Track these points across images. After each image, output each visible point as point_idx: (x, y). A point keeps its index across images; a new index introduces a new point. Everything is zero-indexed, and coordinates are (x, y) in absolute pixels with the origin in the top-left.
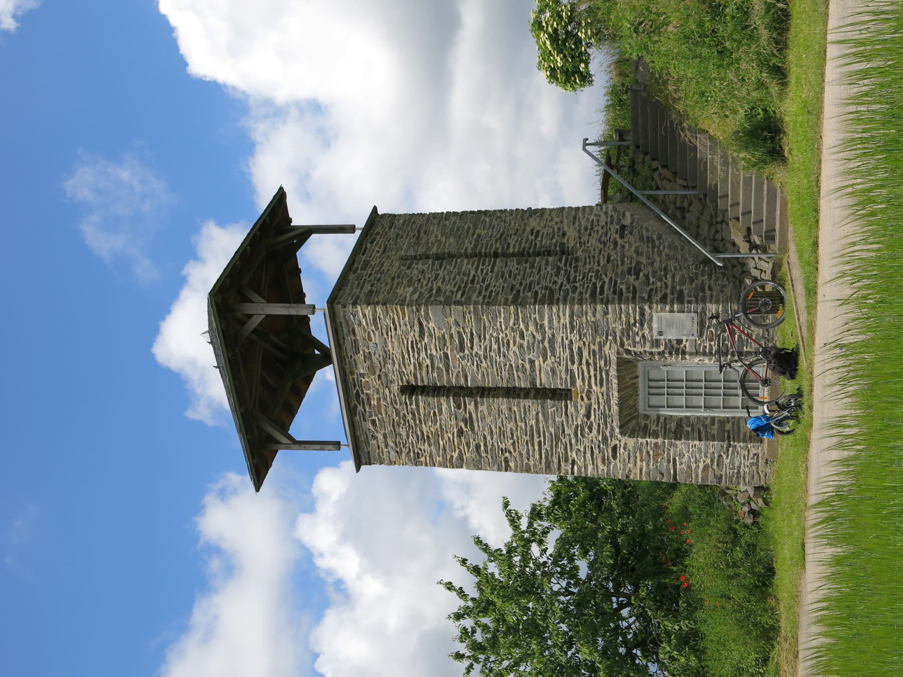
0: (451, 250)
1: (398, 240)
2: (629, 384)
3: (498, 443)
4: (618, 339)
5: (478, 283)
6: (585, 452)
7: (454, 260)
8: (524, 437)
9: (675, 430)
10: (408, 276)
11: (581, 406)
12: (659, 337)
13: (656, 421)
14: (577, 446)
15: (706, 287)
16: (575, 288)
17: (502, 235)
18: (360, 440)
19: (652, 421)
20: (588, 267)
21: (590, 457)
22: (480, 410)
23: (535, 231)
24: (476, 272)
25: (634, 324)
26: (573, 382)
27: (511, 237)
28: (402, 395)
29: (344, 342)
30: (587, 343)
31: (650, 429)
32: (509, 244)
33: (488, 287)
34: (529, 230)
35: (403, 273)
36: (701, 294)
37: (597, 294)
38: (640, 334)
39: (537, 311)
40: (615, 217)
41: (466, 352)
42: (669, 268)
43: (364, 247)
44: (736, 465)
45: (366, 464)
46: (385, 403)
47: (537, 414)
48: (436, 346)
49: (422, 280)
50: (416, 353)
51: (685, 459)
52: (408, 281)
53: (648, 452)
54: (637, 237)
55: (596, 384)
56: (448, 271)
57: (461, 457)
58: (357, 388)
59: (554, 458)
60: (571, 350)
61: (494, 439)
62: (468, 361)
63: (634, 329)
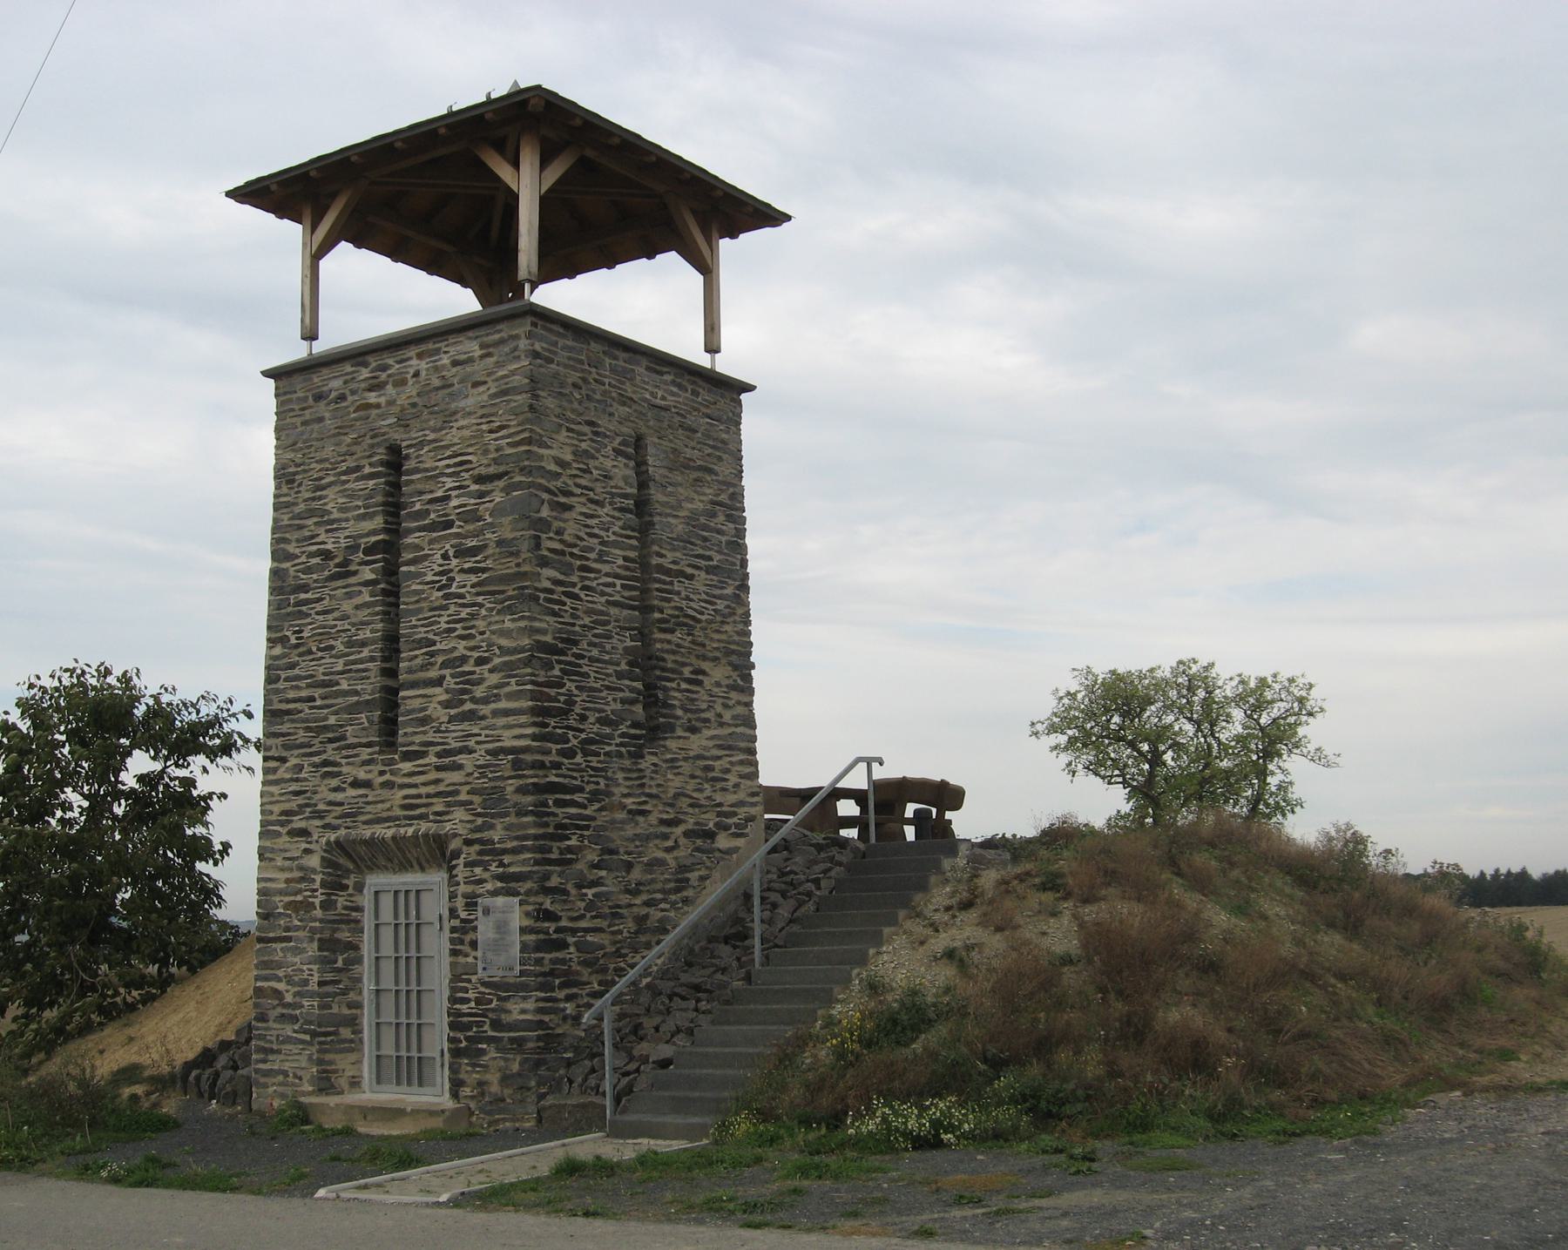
0: (657, 527)
1: (680, 431)
2: (409, 855)
3: (310, 624)
6: (297, 780)
7: (636, 534)
8: (321, 670)
9: (339, 941)
10: (598, 451)
12: (480, 909)
14: (309, 765)
15: (575, 990)
17: (693, 618)
18: (314, 376)
19: (352, 899)
20: (620, 776)
21: (290, 789)
22: (363, 589)
23: (700, 677)
24: (607, 575)
25: (501, 864)
26: (407, 756)
27: (689, 635)
28: (387, 448)
29: (470, 338)
30: (470, 779)
31: (337, 895)
32: (672, 631)
33: (576, 597)
35: (606, 441)
36: (557, 981)
37: (557, 796)
38: (486, 875)
39: (521, 688)
40: (735, 820)
41: (455, 562)
42: (617, 922)
43: (665, 369)
44: (283, 1047)
46: (372, 416)
47: (356, 693)
48: (465, 505)
50: (452, 470)
51: (290, 959)
53: (299, 892)
54: (688, 862)
55: (406, 797)
56: (609, 522)
57: (290, 557)
58: (397, 366)
59: (288, 725)
60: (461, 751)
61: (317, 617)
63: (494, 864)
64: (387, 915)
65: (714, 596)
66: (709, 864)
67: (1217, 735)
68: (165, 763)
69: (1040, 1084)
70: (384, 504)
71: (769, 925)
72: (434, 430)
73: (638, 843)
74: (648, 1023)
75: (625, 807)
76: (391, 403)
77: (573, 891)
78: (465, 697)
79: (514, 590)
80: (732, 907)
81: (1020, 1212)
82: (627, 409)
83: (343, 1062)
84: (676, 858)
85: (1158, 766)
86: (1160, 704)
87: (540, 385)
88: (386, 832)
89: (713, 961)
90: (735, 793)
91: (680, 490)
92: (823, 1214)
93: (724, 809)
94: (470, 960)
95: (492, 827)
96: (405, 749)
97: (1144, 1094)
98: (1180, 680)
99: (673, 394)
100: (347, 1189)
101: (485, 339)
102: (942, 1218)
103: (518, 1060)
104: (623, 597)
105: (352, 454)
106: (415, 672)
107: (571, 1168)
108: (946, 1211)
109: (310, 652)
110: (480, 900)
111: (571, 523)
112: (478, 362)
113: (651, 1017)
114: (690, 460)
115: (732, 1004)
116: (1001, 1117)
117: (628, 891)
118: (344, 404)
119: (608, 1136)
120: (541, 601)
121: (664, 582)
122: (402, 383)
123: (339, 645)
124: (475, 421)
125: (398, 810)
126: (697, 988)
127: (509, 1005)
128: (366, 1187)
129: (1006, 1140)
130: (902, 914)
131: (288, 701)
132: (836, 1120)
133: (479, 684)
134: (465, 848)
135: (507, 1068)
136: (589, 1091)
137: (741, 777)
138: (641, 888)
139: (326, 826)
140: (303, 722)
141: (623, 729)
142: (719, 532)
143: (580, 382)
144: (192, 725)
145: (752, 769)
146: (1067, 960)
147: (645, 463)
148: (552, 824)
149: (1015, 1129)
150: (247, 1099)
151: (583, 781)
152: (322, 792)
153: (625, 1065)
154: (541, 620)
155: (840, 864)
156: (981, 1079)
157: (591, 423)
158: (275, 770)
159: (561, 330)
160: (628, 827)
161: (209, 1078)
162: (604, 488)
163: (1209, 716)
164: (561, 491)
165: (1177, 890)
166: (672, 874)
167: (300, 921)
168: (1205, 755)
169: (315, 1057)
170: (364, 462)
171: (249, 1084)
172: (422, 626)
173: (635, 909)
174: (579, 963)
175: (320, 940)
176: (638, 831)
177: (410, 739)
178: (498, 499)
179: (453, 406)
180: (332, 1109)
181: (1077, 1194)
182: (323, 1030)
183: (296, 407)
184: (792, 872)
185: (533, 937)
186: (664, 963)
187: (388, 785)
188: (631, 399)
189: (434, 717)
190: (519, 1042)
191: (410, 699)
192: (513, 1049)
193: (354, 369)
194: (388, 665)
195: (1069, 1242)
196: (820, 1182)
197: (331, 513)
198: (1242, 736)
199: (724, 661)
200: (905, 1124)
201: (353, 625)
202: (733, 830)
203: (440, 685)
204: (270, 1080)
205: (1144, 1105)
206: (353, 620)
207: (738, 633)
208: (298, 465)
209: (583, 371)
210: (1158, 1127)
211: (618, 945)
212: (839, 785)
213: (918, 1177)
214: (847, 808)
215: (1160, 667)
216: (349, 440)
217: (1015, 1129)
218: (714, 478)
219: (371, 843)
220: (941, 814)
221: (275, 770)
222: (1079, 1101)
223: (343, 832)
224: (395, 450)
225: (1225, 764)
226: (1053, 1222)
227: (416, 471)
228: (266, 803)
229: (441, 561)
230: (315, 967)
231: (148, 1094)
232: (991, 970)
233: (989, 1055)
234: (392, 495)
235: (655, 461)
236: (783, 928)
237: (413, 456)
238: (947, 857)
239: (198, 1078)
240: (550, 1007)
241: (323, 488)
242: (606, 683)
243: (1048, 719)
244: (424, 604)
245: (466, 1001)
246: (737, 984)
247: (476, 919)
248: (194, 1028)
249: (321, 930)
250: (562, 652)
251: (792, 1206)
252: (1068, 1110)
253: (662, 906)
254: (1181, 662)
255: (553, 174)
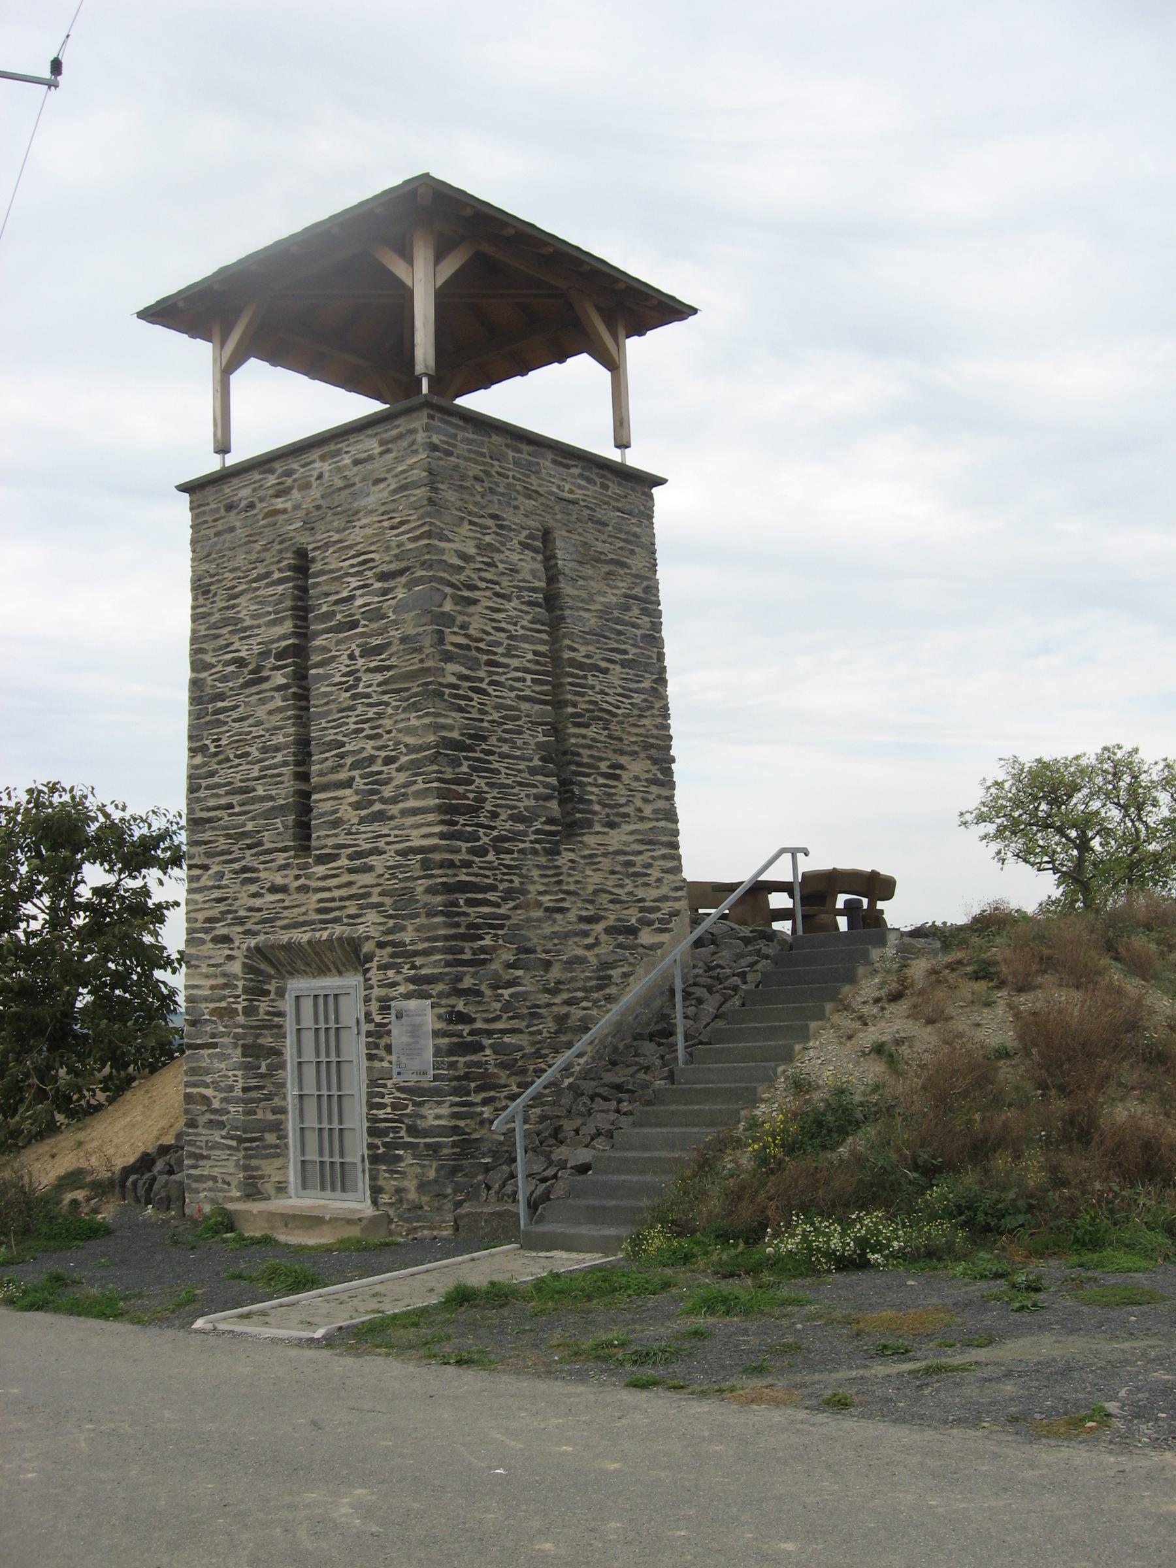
2: (326, 960)
3: (228, 731)
4: (390, 938)
5: (491, 673)
6: (219, 887)
7: (546, 628)
8: (239, 776)
9: (261, 1046)
10: (503, 544)
11: (286, 876)
12: (393, 1012)
13: (275, 1010)
15: (492, 1093)
16: (481, 852)
17: (609, 712)
18: (224, 487)
19: (274, 1004)
20: (535, 873)
21: (213, 896)
22: (276, 694)
23: (618, 772)
24: (516, 669)
25: (413, 967)
26: (322, 860)
27: (605, 729)
29: (369, 436)
31: (259, 1001)
32: (587, 726)
34: (621, 762)
35: (512, 534)
36: (473, 1085)
37: (469, 895)
38: (399, 978)
40: (659, 915)
41: (361, 661)
42: (536, 1022)
45: (191, 502)
47: (272, 798)
48: (368, 604)
49: (492, 569)
52: (490, 545)
53: (223, 998)
54: (610, 959)
55: (321, 901)
56: (517, 617)
57: (207, 667)
58: (302, 470)
61: (233, 724)
62: (348, 666)
63: (407, 966)
64: (308, 1021)
65: (631, 690)
66: (632, 961)
67: (1144, 819)
68: (120, 875)
69: (976, 1196)
70: (293, 608)
71: (694, 1020)
72: (338, 532)
73: (556, 941)
74: (568, 1126)
75: (542, 904)
76: (296, 507)
77: (489, 993)
78: (375, 797)
79: (418, 686)
80: (657, 1004)
81: (955, 1369)
82: (534, 503)
83: (268, 1168)
84: (597, 955)
85: (1087, 851)
86: (1085, 791)
87: (438, 478)
88: (302, 936)
89: (637, 1059)
90: (658, 887)
91: (592, 583)
92: (723, 1367)
93: (646, 904)
94: (385, 1064)
95: (403, 929)
96: (318, 852)
97: (1093, 1206)
98: (1106, 766)
99: (581, 487)
100: (225, 1320)
101: (384, 436)
102: (862, 1378)
103: (434, 1167)
104: (533, 691)
105: (262, 561)
106: (326, 774)
107: (462, 1297)
108: (866, 1367)
109: (228, 760)
110: (393, 1003)
111: (476, 617)
112: (377, 459)
113: (572, 1119)
114: (601, 553)
115: (654, 1105)
116: (934, 1233)
117: (547, 991)
118: (252, 513)
119: (521, 1248)
120: (446, 697)
121: (578, 677)
122: (307, 486)
123: (255, 753)
124: (376, 519)
125: (313, 913)
126: (619, 1088)
127: (424, 1111)
128: (247, 1316)
129: (940, 1259)
130: (829, 1006)
131: (209, 809)
132: (754, 1235)
133: (387, 784)
134: (378, 951)
135: (423, 1175)
136: (506, 1198)
137: (664, 871)
138: (561, 987)
139: (247, 932)
140: (223, 829)
141: (537, 825)
142: (634, 625)
143: (482, 474)
144: (143, 837)
145: (675, 863)
146: (1003, 1053)
147: (554, 557)
148: (464, 924)
149: (950, 1247)
150: (180, 1203)
151: (495, 880)
152: (242, 898)
153: (544, 1171)
154: (446, 716)
155: (767, 957)
156: (911, 1188)
157: (494, 517)
158: (197, 878)
159: (461, 423)
160: (545, 925)
161: (145, 1183)
162: (511, 581)
163: (1136, 802)
164: (464, 585)
165: (1116, 975)
166: (593, 971)
167: (225, 1027)
168: (1134, 841)
169: (241, 1163)
170: (273, 568)
171: (182, 1187)
172: (332, 728)
173: (555, 1009)
174: (496, 1065)
175: (243, 1046)
176: (556, 929)
177: (323, 842)
178: (401, 596)
179: (355, 505)
180: (255, 1215)
181: (1021, 1342)
182: (248, 1135)
183: (209, 519)
184: (718, 966)
185: (446, 1040)
186: (587, 1063)
187: (303, 889)
188: (536, 492)
189: (345, 819)
190: (435, 1148)
191: (322, 802)
192: (427, 1155)
193: (262, 476)
194: (301, 769)
195: (1013, 1420)
196: (728, 1319)
197: (244, 620)
198: (1169, 819)
199: (642, 755)
200: (827, 1242)
201: (267, 730)
202: (657, 925)
203: (350, 787)
204: (201, 1186)
205: (1093, 1219)
206: (267, 726)
207: (656, 727)
208: (212, 576)
209: (485, 464)
210: (1111, 1244)
211: (538, 1046)
212: (762, 878)
213: (838, 1314)
214: (779, 901)
215: (1085, 754)
216: (259, 548)
217: (950, 1247)
218: (628, 571)
219: (288, 947)
220: (872, 904)
221: (197, 878)
222: (1020, 1213)
223: (262, 937)
224: (302, 553)
225: (1153, 847)
226: (995, 1385)
227: (322, 573)
228: (191, 911)
229: (348, 662)
230: (238, 1073)
231: (89, 1199)
232: (922, 1067)
233: (920, 1162)
234: (300, 599)
235: (564, 554)
236: (708, 1024)
237: (318, 558)
238: (874, 947)
239: (135, 1183)
240: (466, 1112)
241: (236, 597)
242: (519, 779)
243: (976, 809)
244: (333, 706)
245: (382, 1106)
246: (660, 1084)
247: (390, 1023)
248: (139, 1133)
249: (244, 1036)
250: (470, 749)
251: (690, 1355)
252: (1009, 1222)
253: (584, 1004)
254: (1105, 749)
255: (449, 268)
